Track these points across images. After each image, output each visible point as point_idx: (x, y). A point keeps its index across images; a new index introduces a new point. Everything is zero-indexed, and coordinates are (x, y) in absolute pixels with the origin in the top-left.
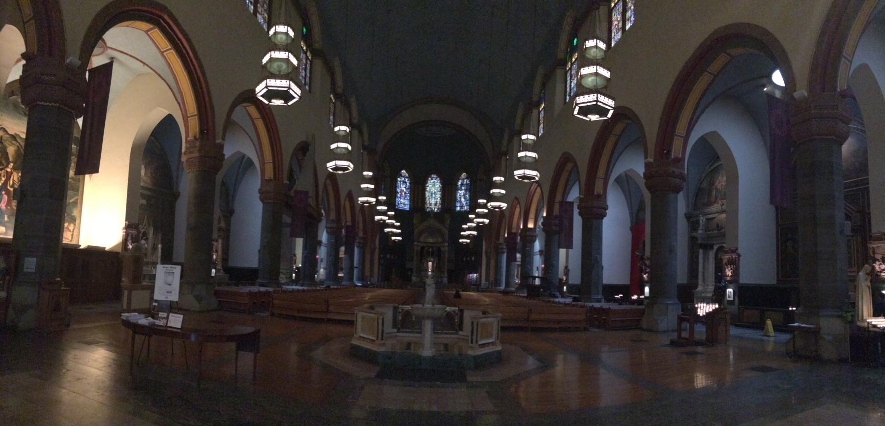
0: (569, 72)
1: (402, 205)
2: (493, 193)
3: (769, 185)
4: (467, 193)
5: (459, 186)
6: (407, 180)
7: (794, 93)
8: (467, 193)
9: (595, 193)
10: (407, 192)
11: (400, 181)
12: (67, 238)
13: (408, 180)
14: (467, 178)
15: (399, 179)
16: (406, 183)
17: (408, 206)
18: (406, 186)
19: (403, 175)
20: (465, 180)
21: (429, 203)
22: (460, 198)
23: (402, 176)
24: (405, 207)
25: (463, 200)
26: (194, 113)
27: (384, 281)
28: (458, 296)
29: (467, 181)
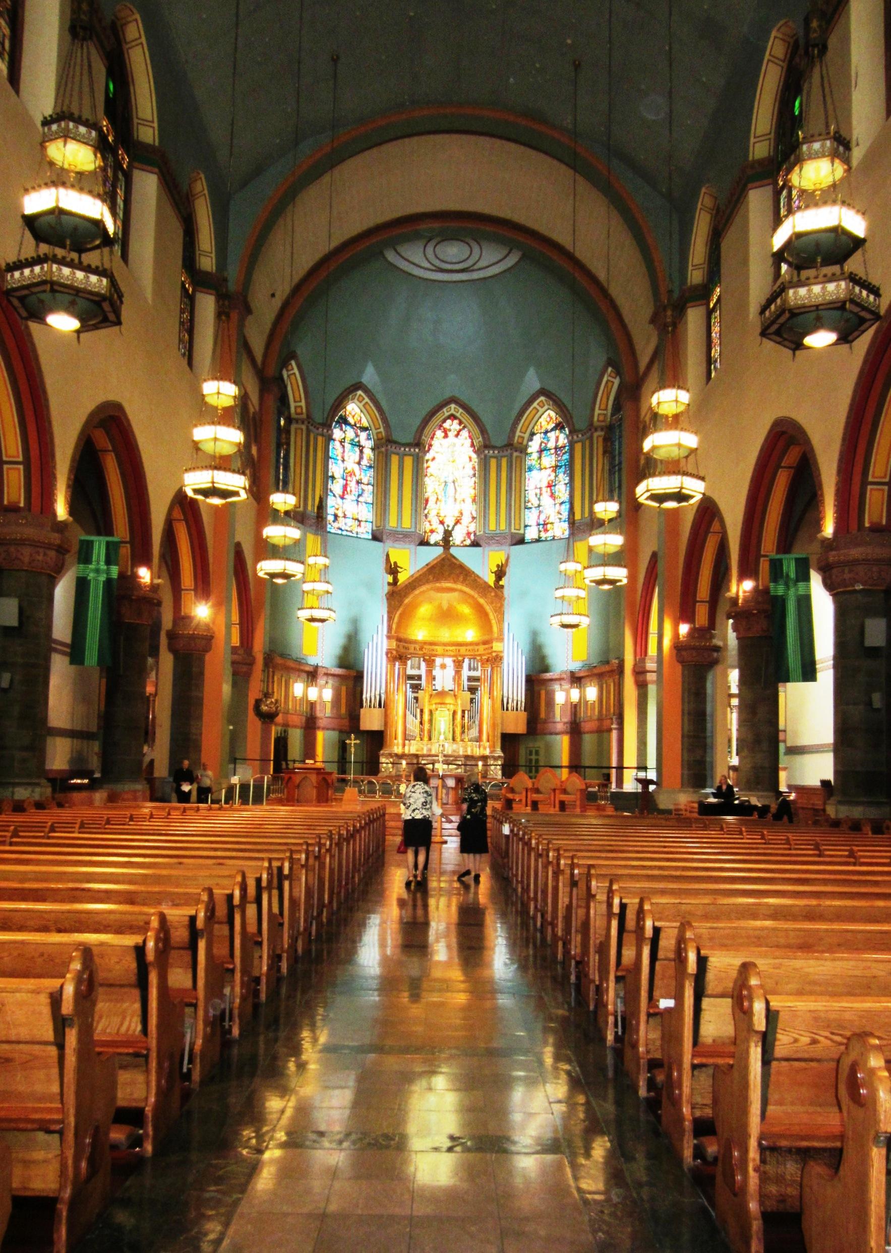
0: (785, 193)
1: (350, 522)
2: (654, 448)
3: (885, 635)
4: (561, 476)
5: (535, 456)
6: (363, 435)
7: (121, 1072)
8: (561, 476)
9: (867, 525)
10: (365, 481)
11: (342, 442)
12: (48, 767)
13: (368, 439)
14: (559, 427)
15: (337, 433)
16: (361, 448)
17: (369, 526)
18: (361, 458)
19: (351, 420)
20: (552, 435)
21: (438, 515)
22: (539, 496)
23: (346, 422)
24: (360, 530)
25: (546, 500)
26: (8, 469)
27: (405, 795)
28: (703, 1128)
29: (557, 438)
